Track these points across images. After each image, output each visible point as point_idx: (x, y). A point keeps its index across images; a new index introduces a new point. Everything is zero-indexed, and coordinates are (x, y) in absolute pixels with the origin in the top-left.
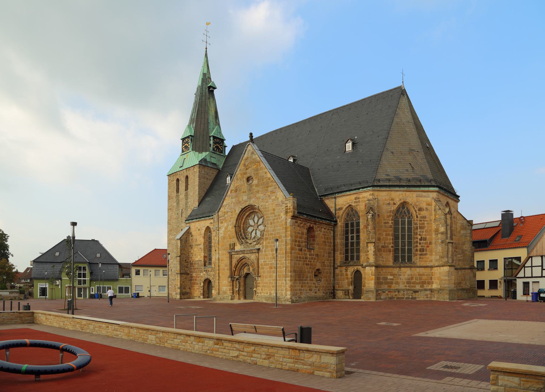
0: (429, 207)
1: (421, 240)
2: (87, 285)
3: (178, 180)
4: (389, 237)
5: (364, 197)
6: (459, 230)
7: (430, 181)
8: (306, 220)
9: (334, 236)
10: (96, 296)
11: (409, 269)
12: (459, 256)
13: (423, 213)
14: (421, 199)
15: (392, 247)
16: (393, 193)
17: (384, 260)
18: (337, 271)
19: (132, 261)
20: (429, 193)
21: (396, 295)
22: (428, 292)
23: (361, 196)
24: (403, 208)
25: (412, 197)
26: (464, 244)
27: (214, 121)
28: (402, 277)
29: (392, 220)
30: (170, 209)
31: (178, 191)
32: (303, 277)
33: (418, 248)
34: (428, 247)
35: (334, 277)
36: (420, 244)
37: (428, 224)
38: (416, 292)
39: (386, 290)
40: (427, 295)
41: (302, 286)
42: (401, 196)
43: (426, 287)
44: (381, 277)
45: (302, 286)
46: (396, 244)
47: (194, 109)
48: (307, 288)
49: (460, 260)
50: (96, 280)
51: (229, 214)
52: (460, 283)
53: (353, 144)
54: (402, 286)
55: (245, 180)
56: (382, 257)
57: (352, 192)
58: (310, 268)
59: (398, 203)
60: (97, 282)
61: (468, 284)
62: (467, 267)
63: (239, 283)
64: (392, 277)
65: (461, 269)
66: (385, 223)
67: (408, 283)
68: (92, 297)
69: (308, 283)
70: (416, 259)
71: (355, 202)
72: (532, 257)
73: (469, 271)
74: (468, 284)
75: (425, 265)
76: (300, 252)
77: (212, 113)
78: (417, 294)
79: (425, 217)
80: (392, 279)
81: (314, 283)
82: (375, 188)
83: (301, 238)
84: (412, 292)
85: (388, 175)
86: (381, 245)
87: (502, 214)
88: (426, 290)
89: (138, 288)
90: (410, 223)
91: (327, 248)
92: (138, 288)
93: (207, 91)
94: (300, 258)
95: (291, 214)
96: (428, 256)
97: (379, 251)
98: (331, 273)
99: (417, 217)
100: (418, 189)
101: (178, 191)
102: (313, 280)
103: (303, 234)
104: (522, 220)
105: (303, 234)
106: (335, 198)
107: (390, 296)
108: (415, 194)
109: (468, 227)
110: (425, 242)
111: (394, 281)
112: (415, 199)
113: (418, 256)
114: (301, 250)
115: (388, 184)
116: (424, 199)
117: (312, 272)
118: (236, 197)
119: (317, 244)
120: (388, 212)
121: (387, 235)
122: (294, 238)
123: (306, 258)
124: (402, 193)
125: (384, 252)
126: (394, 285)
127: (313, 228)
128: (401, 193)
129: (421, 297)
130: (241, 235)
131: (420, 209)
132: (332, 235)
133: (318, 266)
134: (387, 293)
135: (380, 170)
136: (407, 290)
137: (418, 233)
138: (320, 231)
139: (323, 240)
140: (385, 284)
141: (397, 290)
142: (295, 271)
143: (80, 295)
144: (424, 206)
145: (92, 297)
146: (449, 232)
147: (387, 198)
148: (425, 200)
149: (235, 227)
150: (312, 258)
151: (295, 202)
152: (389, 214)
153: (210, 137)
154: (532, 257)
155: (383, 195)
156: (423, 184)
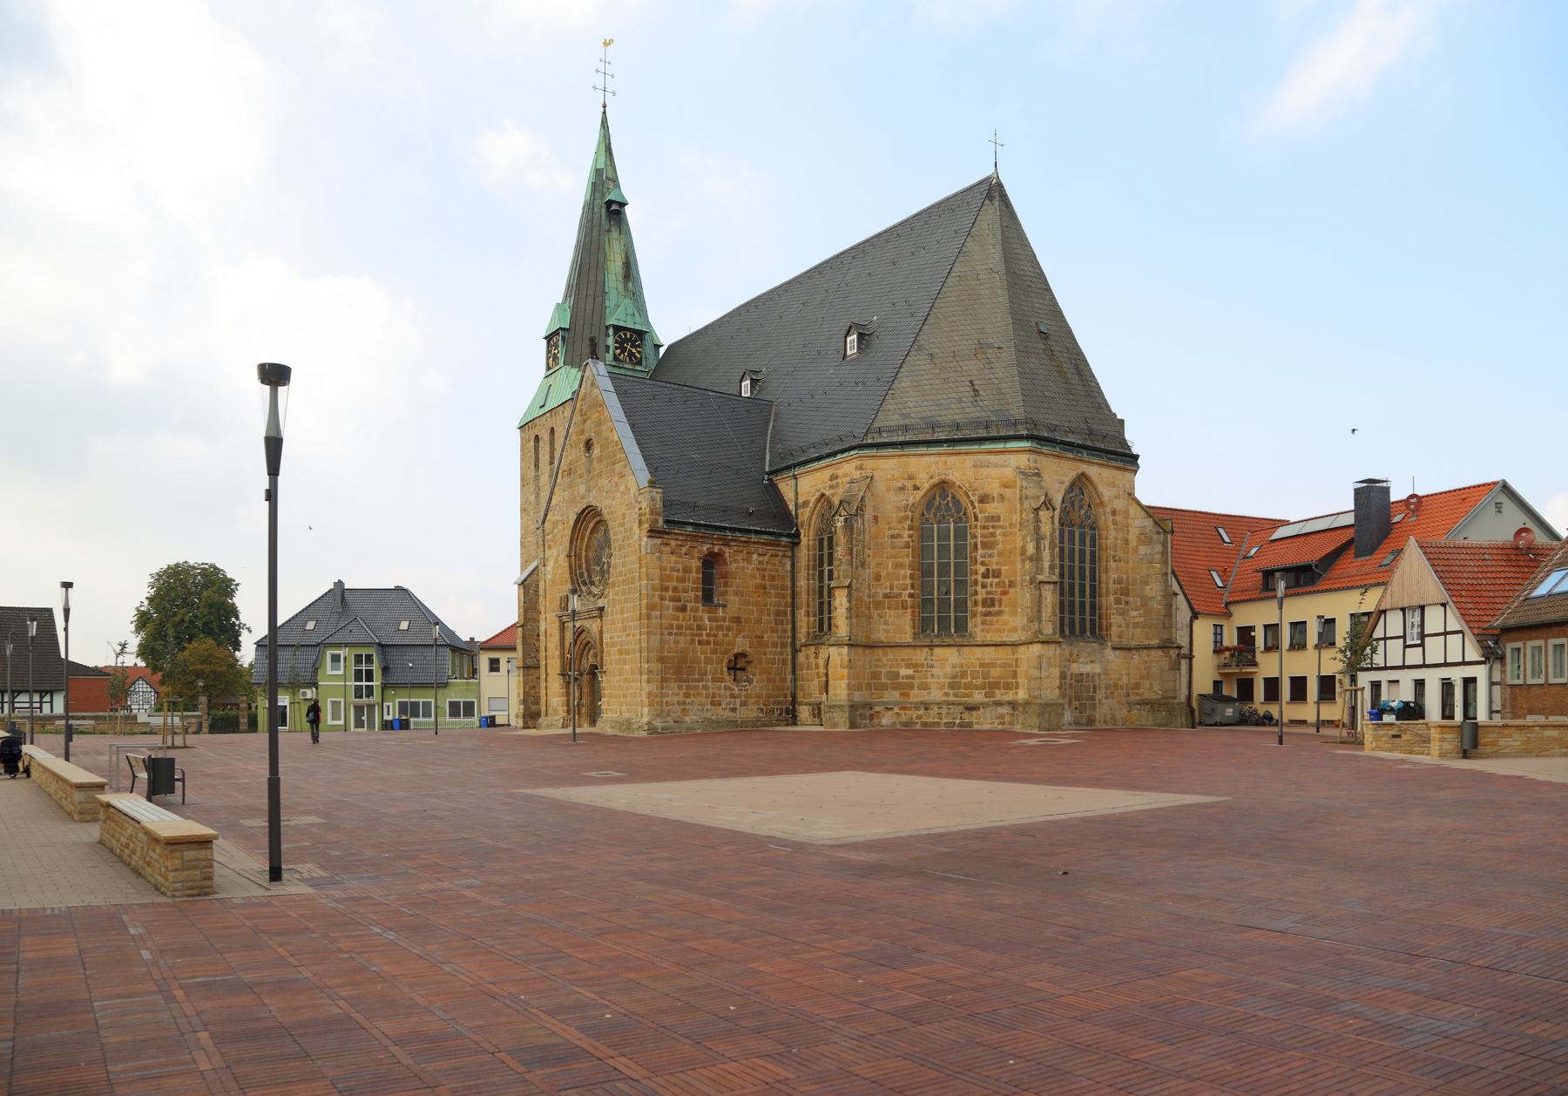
0: (1007, 492)
1: (985, 576)
2: (376, 698)
3: (537, 438)
5: (845, 475)
6: (1133, 543)
7: (1015, 425)
8: (694, 538)
9: (793, 572)
10: (396, 724)
11: (954, 649)
12: (1134, 613)
14: (985, 471)
15: (911, 596)
16: (912, 460)
17: (891, 628)
18: (801, 657)
19: (482, 637)
22: (1005, 710)
23: (840, 472)
24: (944, 495)
25: (961, 468)
26: (1146, 583)
27: (621, 287)
29: (910, 528)
30: (524, 510)
31: (537, 466)
32: (692, 673)
33: (979, 598)
34: (1005, 593)
35: (794, 672)
36: (984, 586)
37: (1005, 534)
38: (971, 708)
39: (895, 704)
40: (1002, 716)
41: (687, 695)
43: (999, 695)
45: (687, 695)
46: (925, 587)
47: (574, 261)
48: (704, 700)
49: (1136, 625)
50: (396, 686)
51: (560, 527)
52: (1137, 686)
53: (861, 336)
54: (936, 695)
55: (582, 446)
56: (886, 623)
57: (823, 463)
58: (714, 652)
59: (927, 486)
60: (400, 691)
61: (1156, 688)
62: (1155, 642)
63: (580, 688)
64: (910, 672)
65: (1138, 648)
67: (951, 686)
68: (387, 726)
69: (705, 687)
70: (976, 627)
71: (831, 487)
72: (1384, 612)
73: (1160, 653)
74: (1156, 688)
75: (998, 639)
76: (681, 615)
77: (615, 266)
79: (998, 519)
80: (912, 677)
81: (726, 688)
82: (866, 452)
83: (682, 580)
85: (906, 416)
86: (881, 592)
87: (1357, 491)
88: (999, 704)
89: (496, 704)
90: (961, 534)
91: (771, 600)
92: (496, 704)
93: (606, 212)
94: (679, 627)
95: (646, 526)
96: (1005, 617)
98: (784, 662)
100: (975, 447)
101: (537, 466)
102: (722, 680)
103: (687, 570)
104: (1415, 503)
105: (687, 570)
106: (795, 477)
107: (904, 719)
108: (970, 461)
109: (1155, 537)
111: (916, 682)
112: (970, 474)
113: (979, 619)
114: (683, 609)
115: (901, 439)
116: (994, 472)
117: (720, 661)
118: (570, 486)
119: (736, 593)
120: (899, 509)
121: (896, 566)
122: (657, 582)
123: (699, 628)
124: (937, 459)
127: (720, 555)
128: (933, 459)
129: (985, 721)
130: (582, 575)
131: (984, 499)
133: (741, 644)
135: (890, 405)
136: (948, 703)
138: (749, 561)
140: (894, 688)
142: (661, 659)
143: (359, 724)
144: (994, 489)
145: (387, 726)
147: (898, 474)
148: (998, 477)
149: (569, 556)
151: (658, 497)
154: (1384, 612)
155: (887, 467)
156: (993, 434)
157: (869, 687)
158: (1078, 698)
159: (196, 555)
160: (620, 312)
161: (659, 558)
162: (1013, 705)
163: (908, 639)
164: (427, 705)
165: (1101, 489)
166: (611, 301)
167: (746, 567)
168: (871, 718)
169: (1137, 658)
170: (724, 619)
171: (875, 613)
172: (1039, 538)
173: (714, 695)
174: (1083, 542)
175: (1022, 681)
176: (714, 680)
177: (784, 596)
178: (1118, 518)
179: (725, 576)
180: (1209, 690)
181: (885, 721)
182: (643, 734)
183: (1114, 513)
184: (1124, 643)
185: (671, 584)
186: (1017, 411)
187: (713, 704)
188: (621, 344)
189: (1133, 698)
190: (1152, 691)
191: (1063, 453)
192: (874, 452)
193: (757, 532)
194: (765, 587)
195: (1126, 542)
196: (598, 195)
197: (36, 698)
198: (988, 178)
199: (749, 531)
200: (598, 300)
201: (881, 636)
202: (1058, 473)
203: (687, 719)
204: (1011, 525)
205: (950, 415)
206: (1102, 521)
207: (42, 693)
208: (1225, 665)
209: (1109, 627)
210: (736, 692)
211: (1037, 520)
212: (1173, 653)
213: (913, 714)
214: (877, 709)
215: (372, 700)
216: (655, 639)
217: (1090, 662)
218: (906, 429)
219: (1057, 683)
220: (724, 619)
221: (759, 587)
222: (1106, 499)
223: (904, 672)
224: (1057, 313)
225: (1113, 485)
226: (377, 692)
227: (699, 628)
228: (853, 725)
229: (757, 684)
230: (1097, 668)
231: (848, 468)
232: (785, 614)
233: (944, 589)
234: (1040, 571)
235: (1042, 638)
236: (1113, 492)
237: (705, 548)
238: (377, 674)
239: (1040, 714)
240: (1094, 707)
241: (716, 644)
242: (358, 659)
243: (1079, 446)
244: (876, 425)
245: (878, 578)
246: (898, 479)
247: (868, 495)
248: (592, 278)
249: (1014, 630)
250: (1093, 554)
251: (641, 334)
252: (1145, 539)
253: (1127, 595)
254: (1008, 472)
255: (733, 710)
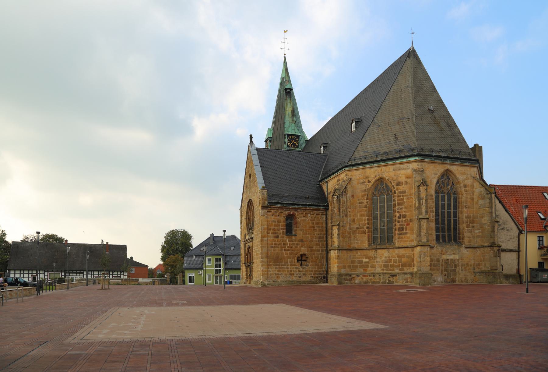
1: (399, 218)
2: (222, 274)
4: (364, 218)
5: (342, 179)
6: (476, 199)
8: (282, 209)
11: (386, 250)
12: (477, 231)
13: (401, 188)
14: (399, 172)
15: (368, 228)
16: (367, 170)
17: (359, 242)
20: (408, 165)
21: (371, 279)
22: (408, 276)
23: (340, 178)
25: (388, 172)
26: (482, 217)
27: (291, 120)
28: (378, 260)
29: (367, 199)
33: (397, 227)
34: (408, 225)
35: (327, 261)
36: (399, 222)
37: (408, 199)
38: (393, 276)
39: (361, 274)
40: (407, 279)
41: (279, 271)
42: (376, 173)
43: (406, 270)
44: (356, 260)
45: (279, 271)
49: (478, 237)
52: (479, 264)
54: (378, 270)
56: (357, 240)
58: (291, 253)
59: (374, 180)
60: (230, 271)
61: (488, 265)
62: (487, 244)
64: (367, 260)
65: (479, 247)
66: (360, 203)
67: (385, 266)
69: (287, 268)
70: (397, 242)
73: (489, 249)
75: (405, 245)
76: (276, 239)
77: (289, 112)
78: (395, 278)
79: (405, 192)
80: (368, 262)
83: (277, 225)
84: (389, 276)
88: (406, 273)
90: (390, 200)
93: (286, 92)
96: (408, 235)
97: (353, 234)
99: (395, 193)
100: (394, 162)
103: (279, 221)
105: (279, 221)
106: (327, 182)
107: (364, 280)
108: (392, 168)
109: (486, 196)
110: (404, 219)
111: (370, 264)
113: (397, 236)
114: (277, 237)
115: (363, 161)
116: (403, 172)
117: (294, 257)
119: (301, 230)
120: (362, 191)
121: (361, 215)
122: (266, 227)
125: (358, 234)
126: (369, 269)
128: (376, 169)
131: (398, 184)
132: (325, 219)
133: (303, 251)
134: (361, 277)
136: (383, 273)
137: (397, 210)
138: (307, 217)
139: (311, 225)
140: (360, 267)
141: (373, 273)
142: (267, 257)
143: (216, 282)
144: (403, 179)
145: (226, 283)
146: (424, 206)
147: (361, 176)
150: (293, 244)
151: (266, 193)
152: (363, 193)
153: (285, 135)
155: (357, 174)
156: (402, 155)
157: (350, 267)
158: (446, 270)
159: (179, 227)
160: (290, 130)
161: (267, 217)
162: (412, 274)
163: (366, 246)
164: (239, 276)
165: (458, 176)
166: (287, 125)
167: (305, 220)
168: (350, 280)
169: (478, 251)
170: (295, 241)
171: (353, 236)
172: (420, 199)
173: (291, 271)
174: (449, 200)
175: (415, 263)
176: (291, 265)
177: (322, 231)
178: (467, 188)
179: (296, 223)
180: (536, 266)
181: (356, 281)
182: (260, 286)
183: (465, 186)
184: (472, 245)
185: (272, 228)
186: (414, 145)
187: (290, 274)
188: (290, 141)
189: (477, 270)
190: (486, 267)
191: (436, 161)
192: (351, 168)
193: (309, 205)
194: (314, 227)
195: (472, 199)
196: (282, 87)
197: (119, 273)
198: (410, 49)
199: (306, 205)
200: (282, 125)
201: (355, 245)
202: (433, 171)
203: (279, 280)
204: (411, 195)
205: (383, 150)
206: (459, 190)
207: (121, 272)
208: (545, 255)
209: (464, 237)
210: (301, 269)
211: (419, 191)
212: (496, 249)
213: (368, 278)
214: (354, 276)
215: (221, 274)
216: (265, 250)
217: (451, 254)
218: (365, 157)
219: (429, 263)
220: (295, 241)
221: (311, 227)
222: (461, 180)
223: (365, 260)
224: (439, 101)
225: (465, 174)
226: (222, 271)
227: (284, 244)
228: (340, 283)
229: (310, 266)
230: (457, 257)
231: (343, 176)
232: (323, 238)
233: (382, 224)
234: (420, 213)
235: (421, 243)
236: (465, 177)
237: (287, 213)
238: (223, 265)
239: (420, 278)
240: (455, 274)
241: (292, 250)
242: (216, 260)
243: (445, 157)
244: (353, 157)
245: (354, 221)
246: (361, 178)
247: (349, 186)
248: (280, 118)
249: (412, 241)
250: (455, 206)
251: (298, 136)
252: (481, 197)
253: (473, 223)
254: (409, 171)
255: (300, 277)
